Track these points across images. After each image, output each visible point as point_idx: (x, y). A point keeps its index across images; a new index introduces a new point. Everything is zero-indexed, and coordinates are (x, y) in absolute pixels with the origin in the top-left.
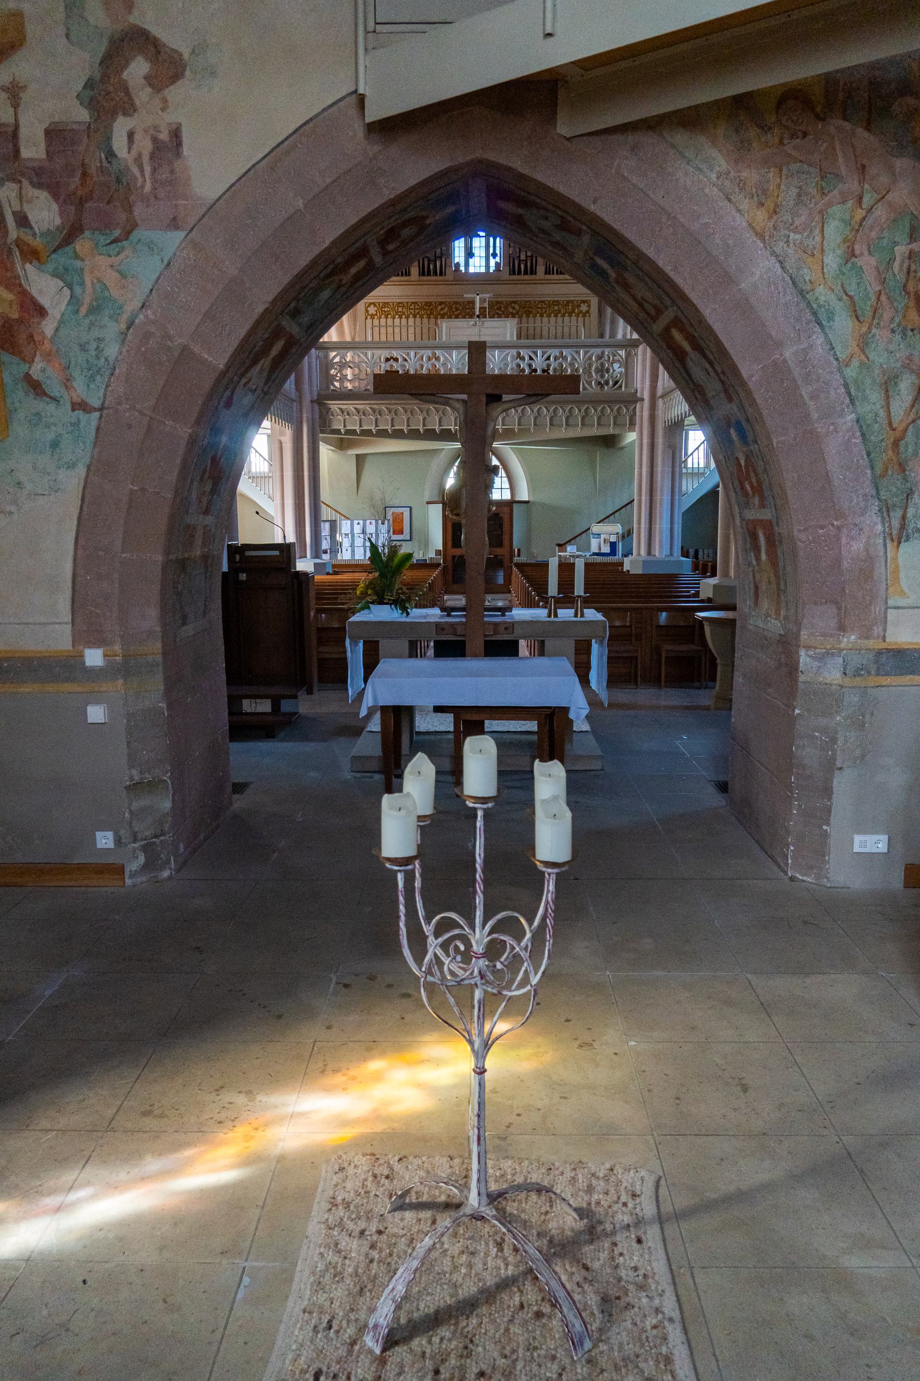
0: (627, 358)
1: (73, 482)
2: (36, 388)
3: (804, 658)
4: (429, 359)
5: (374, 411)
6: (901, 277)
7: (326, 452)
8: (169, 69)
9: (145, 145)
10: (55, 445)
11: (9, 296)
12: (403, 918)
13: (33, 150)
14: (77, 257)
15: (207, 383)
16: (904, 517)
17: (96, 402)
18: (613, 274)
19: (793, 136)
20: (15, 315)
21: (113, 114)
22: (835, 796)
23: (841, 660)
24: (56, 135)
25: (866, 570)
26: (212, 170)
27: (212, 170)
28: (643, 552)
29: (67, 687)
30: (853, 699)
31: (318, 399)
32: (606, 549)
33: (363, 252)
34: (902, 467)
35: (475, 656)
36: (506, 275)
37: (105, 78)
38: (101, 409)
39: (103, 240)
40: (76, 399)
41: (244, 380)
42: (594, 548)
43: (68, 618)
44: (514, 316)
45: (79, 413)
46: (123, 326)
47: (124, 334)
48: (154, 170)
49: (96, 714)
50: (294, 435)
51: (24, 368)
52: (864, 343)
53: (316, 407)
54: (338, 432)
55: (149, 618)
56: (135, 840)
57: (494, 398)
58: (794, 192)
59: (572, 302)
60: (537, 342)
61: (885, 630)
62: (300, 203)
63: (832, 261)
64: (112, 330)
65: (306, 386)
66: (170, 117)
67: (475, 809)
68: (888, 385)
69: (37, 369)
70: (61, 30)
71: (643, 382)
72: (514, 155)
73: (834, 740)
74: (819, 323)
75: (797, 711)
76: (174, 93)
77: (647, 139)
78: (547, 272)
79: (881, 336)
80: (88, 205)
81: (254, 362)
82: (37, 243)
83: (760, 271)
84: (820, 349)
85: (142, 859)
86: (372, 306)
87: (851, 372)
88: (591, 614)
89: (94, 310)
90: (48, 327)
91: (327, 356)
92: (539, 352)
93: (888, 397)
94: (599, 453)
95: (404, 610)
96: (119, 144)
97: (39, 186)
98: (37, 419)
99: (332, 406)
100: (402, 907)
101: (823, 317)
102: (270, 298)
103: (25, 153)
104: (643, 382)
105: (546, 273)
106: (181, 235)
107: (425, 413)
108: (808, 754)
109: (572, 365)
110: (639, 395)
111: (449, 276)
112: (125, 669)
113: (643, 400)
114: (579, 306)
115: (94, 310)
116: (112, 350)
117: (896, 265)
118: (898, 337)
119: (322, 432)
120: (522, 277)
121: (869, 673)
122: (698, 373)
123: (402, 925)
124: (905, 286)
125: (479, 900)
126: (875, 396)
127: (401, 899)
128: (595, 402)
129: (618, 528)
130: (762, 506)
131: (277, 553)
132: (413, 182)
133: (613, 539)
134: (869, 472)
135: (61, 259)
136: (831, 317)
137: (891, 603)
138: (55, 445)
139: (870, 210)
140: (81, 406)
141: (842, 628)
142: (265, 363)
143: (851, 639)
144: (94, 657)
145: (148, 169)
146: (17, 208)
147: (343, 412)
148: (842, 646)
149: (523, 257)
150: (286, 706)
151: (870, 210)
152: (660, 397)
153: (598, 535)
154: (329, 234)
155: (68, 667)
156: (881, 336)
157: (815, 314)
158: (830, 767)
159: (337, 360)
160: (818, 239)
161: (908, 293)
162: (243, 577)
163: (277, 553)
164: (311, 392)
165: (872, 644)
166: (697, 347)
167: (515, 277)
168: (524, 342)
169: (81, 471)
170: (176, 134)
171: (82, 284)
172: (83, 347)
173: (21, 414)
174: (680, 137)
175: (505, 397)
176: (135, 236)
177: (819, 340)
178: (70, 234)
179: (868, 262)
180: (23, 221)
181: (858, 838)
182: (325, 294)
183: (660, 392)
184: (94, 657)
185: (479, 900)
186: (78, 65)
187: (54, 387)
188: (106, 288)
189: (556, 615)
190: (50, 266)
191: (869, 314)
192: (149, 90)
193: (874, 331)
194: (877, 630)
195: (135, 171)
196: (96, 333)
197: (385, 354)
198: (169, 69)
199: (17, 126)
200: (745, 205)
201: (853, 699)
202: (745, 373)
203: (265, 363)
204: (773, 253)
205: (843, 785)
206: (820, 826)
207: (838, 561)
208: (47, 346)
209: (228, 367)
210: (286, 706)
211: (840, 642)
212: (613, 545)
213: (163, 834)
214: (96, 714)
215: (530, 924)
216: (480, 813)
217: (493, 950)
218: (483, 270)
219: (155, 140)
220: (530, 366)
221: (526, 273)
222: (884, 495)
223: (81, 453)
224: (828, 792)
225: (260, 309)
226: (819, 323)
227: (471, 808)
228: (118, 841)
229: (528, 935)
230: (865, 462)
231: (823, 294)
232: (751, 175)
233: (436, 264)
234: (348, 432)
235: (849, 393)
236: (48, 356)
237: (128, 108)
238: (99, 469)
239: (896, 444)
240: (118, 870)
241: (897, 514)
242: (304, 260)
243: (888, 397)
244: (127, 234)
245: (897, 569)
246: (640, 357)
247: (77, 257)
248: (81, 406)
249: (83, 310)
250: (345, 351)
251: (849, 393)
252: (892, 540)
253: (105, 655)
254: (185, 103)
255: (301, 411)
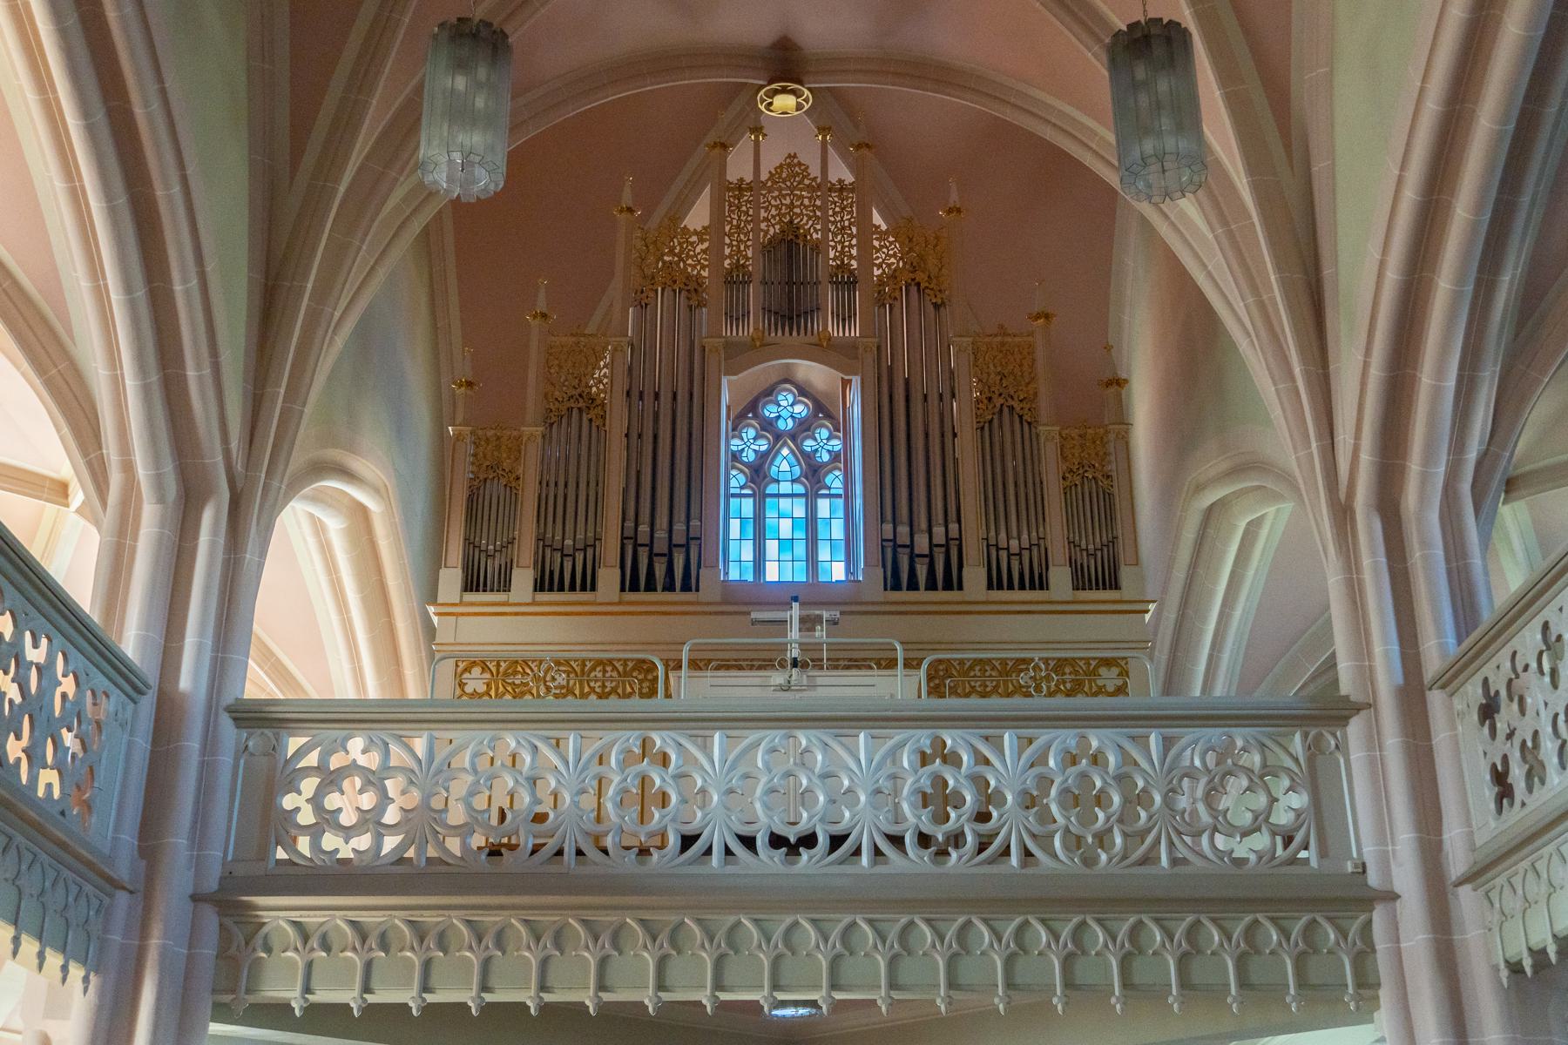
0: (1311, 760)
4: (627, 760)
5: (420, 931)
31: (222, 888)
36: (875, 590)
50: (100, 1008)
53: (211, 919)
59: (1072, 662)
65: (178, 840)
71: (1384, 833)
78: (995, 583)
86: (476, 671)
91: (275, 749)
92: (1008, 738)
99: (266, 916)
104: (1384, 833)
105: (990, 587)
107: (605, 939)
109: (1123, 779)
110: (1373, 879)
111: (708, 589)
113: (1392, 897)
114: (1094, 672)
119: (223, 1013)
120: (922, 595)
147: (305, 938)
149: (922, 544)
152: (1469, 878)
159: (312, 759)
164: (198, 864)
167: (904, 595)
183: (1457, 862)
218: (801, 577)
220: (980, 783)
221: (932, 585)
246: (1357, 754)
250: (336, 733)
255: (144, 934)
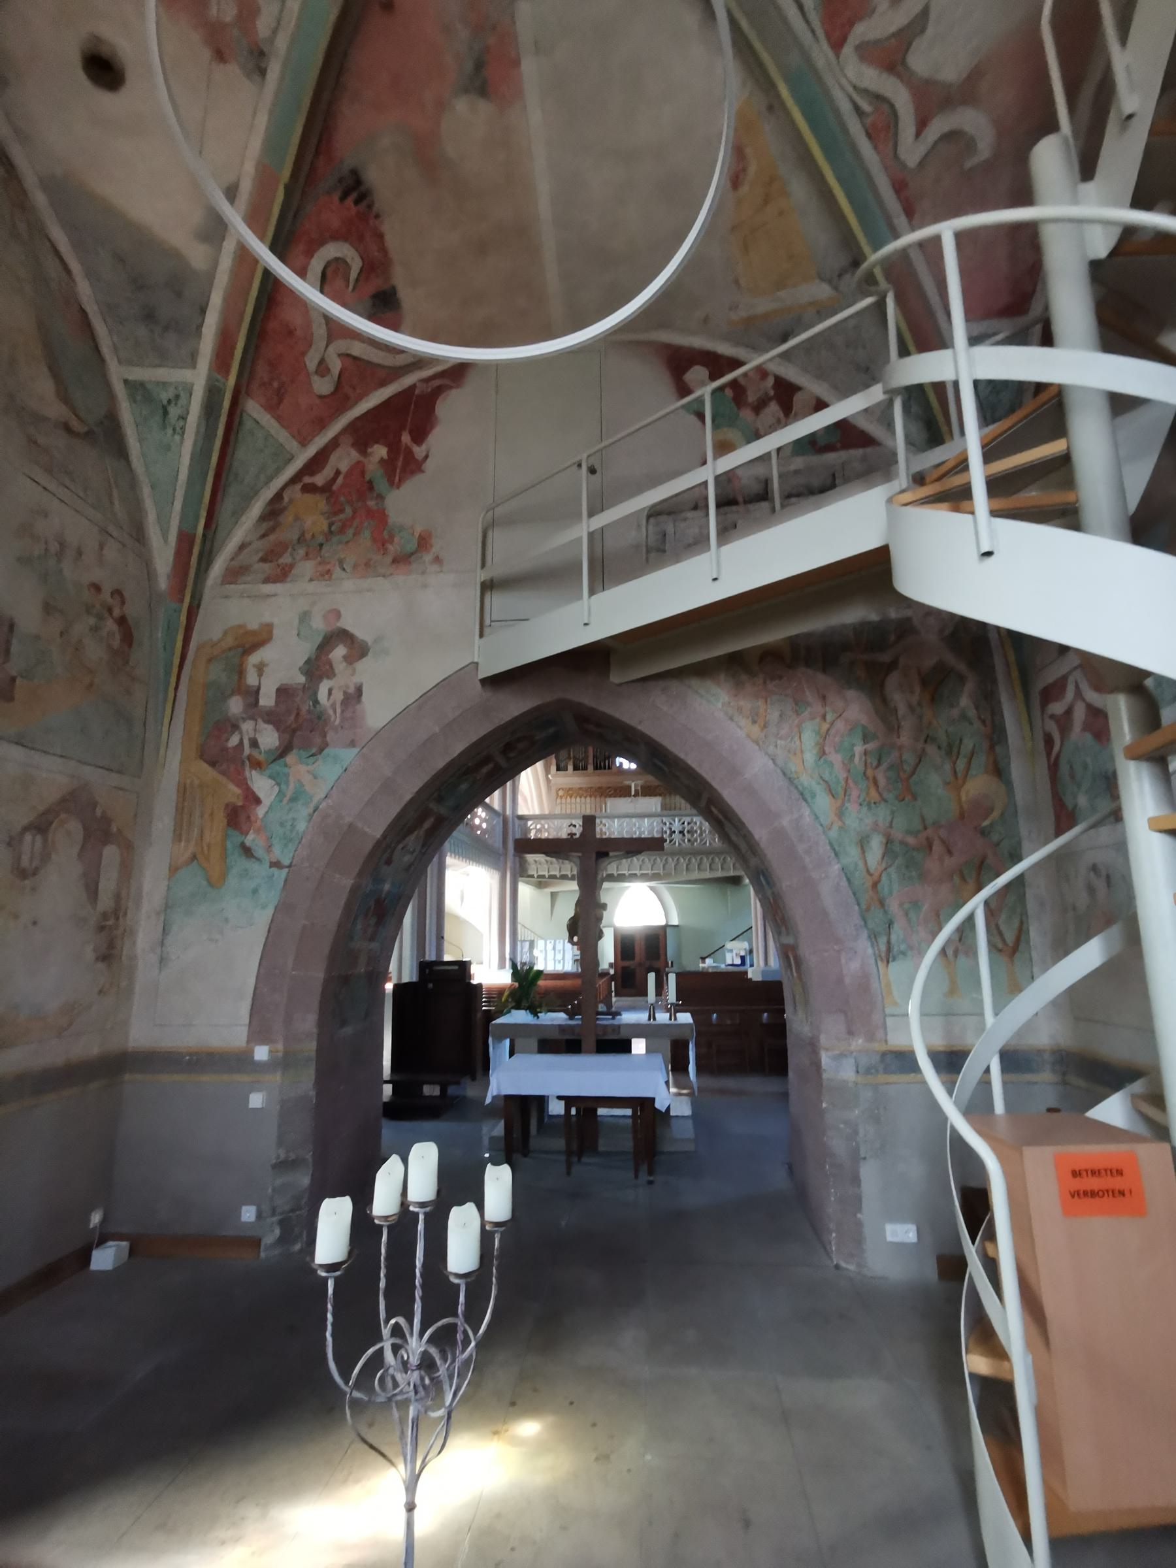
1: (263, 917)
2: (247, 851)
3: (825, 1059)
6: (861, 768)
7: (525, 891)
8: (358, 650)
9: (338, 696)
10: (255, 891)
11: (238, 791)
12: (329, 1327)
13: (267, 700)
14: (286, 765)
15: (368, 847)
16: (889, 942)
17: (286, 862)
18: (666, 769)
19: (772, 679)
20: (240, 803)
21: (320, 678)
22: (863, 1185)
23: (853, 1061)
24: (283, 692)
25: (864, 985)
26: (378, 711)
27: (378, 711)
28: (762, 963)
29: (238, 1077)
30: (867, 1094)
32: (738, 961)
33: (488, 759)
34: (882, 904)
35: (589, 1052)
37: (318, 657)
38: (290, 866)
39: (304, 754)
40: (274, 860)
41: (401, 846)
42: (729, 961)
43: (247, 1021)
44: (660, 795)
45: (274, 869)
46: (311, 810)
47: (311, 816)
48: (343, 711)
49: (256, 1100)
51: (240, 839)
52: (840, 814)
54: (532, 876)
55: (308, 1022)
56: (273, 1214)
57: (602, 855)
58: (776, 714)
60: (673, 812)
61: (886, 1034)
62: (437, 729)
63: (810, 757)
64: (303, 812)
66: (356, 679)
67: (417, 1214)
68: (863, 843)
69: (250, 839)
70: (295, 632)
72: (583, 694)
73: (856, 1133)
74: (806, 800)
75: (824, 1105)
76: (360, 665)
77: (674, 685)
79: (852, 809)
80: (298, 733)
81: (410, 831)
82: (261, 758)
83: (758, 765)
84: (807, 817)
85: (277, 1232)
87: (833, 834)
88: (685, 1018)
89: (294, 799)
90: (261, 811)
93: (863, 852)
94: (730, 890)
95: (535, 1014)
96: (322, 695)
97: (268, 722)
98: (245, 874)
100: (330, 1316)
101: (808, 796)
102: (416, 789)
103: (262, 702)
106: (355, 751)
108: (837, 1144)
111: (614, 770)
112: (285, 1063)
115: (294, 799)
116: (302, 826)
117: (857, 759)
118: (865, 809)
121: (877, 1071)
122: (734, 838)
123: (328, 1335)
124: (865, 773)
125: (418, 1307)
126: (853, 852)
127: (330, 1307)
128: (681, 853)
129: (746, 945)
130: (788, 934)
131: (456, 967)
132: (516, 713)
133: (743, 953)
134: (856, 908)
135: (276, 767)
136: (814, 796)
137: (888, 1011)
138: (255, 891)
139: (832, 724)
140: (276, 864)
141: (850, 1033)
142: (421, 832)
143: (859, 1042)
144: (261, 1053)
145: (339, 710)
146: (252, 735)
148: (852, 1048)
150: (452, 1090)
151: (832, 724)
153: (731, 951)
154: (458, 748)
155: (240, 1061)
156: (852, 809)
157: (802, 794)
158: (856, 1157)
160: (798, 743)
161: (867, 778)
162: (430, 986)
163: (456, 967)
165: (878, 1047)
166: (726, 817)
168: (665, 812)
169: (270, 911)
170: (359, 690)
171: (288, 786)
172: (282, 825)
173: (235, 871)
174: (695, 682)
175: (611, 854)
176: (326, 751)
177: (807, 812)
178: (283, 752)
179: (836, 758)
180: (254, 744)
181: (889, 1228)
182: (464, 786)
184: (261, 1053)
185: (418, 1307)
186: (303, 650)
187: (259, 852)
188: (303, 786)
189: (654, 1019)
190: (268, 772)
191: (840, 791)
192: (344, 664)
193: (847, 805)
194: (880, 1034)
195: (331, 712)
196: (291, 815)
197: (568, 822)
198: (358, 650)
199: (259, 688)
200: (743, 722)
201: (867, 1094)
202: (757, 837)
203: (421, 832)
204: (767, 754)
205: (869, 1174)
206: (855, 1215)
207: (840, 980)
208: (259, 823)
209: (384, 836)
210: (452, 1090)
211: (850, 1045)
212: (743, 958)
213: (300, 1209)
214: (256, 1100)
215: (475, 1333)
216: (421, 1217)
217: (427, 1364)
219: (345, 693)
222: (871, 925)
223: (271, 897)
224: (856, 1180)
225: (408, 797)
226: (806, 800)
227: (413, 1212)
228: (259, 1215)
229: (473, 1344)
230: (852, 900)
231: (806, 780)
232: (746, 704)
233: (603, 764)
234: (539, 876)
235: (834, 850)
236: (258, 831)
237: (330, 673)
238: (284, 908)
239: (875, 885)
240: (256, 1243)
241: (882, 940)
242: (441, 764)
243: (863, 852)
244: (321, 750)
245: (888, 985)
247: (286, 765)
248: (276, 864)
249: (285, 802)
251: (834, 850)
252: (882, 960)
253: (270, 1051)
254: (366, 672)
